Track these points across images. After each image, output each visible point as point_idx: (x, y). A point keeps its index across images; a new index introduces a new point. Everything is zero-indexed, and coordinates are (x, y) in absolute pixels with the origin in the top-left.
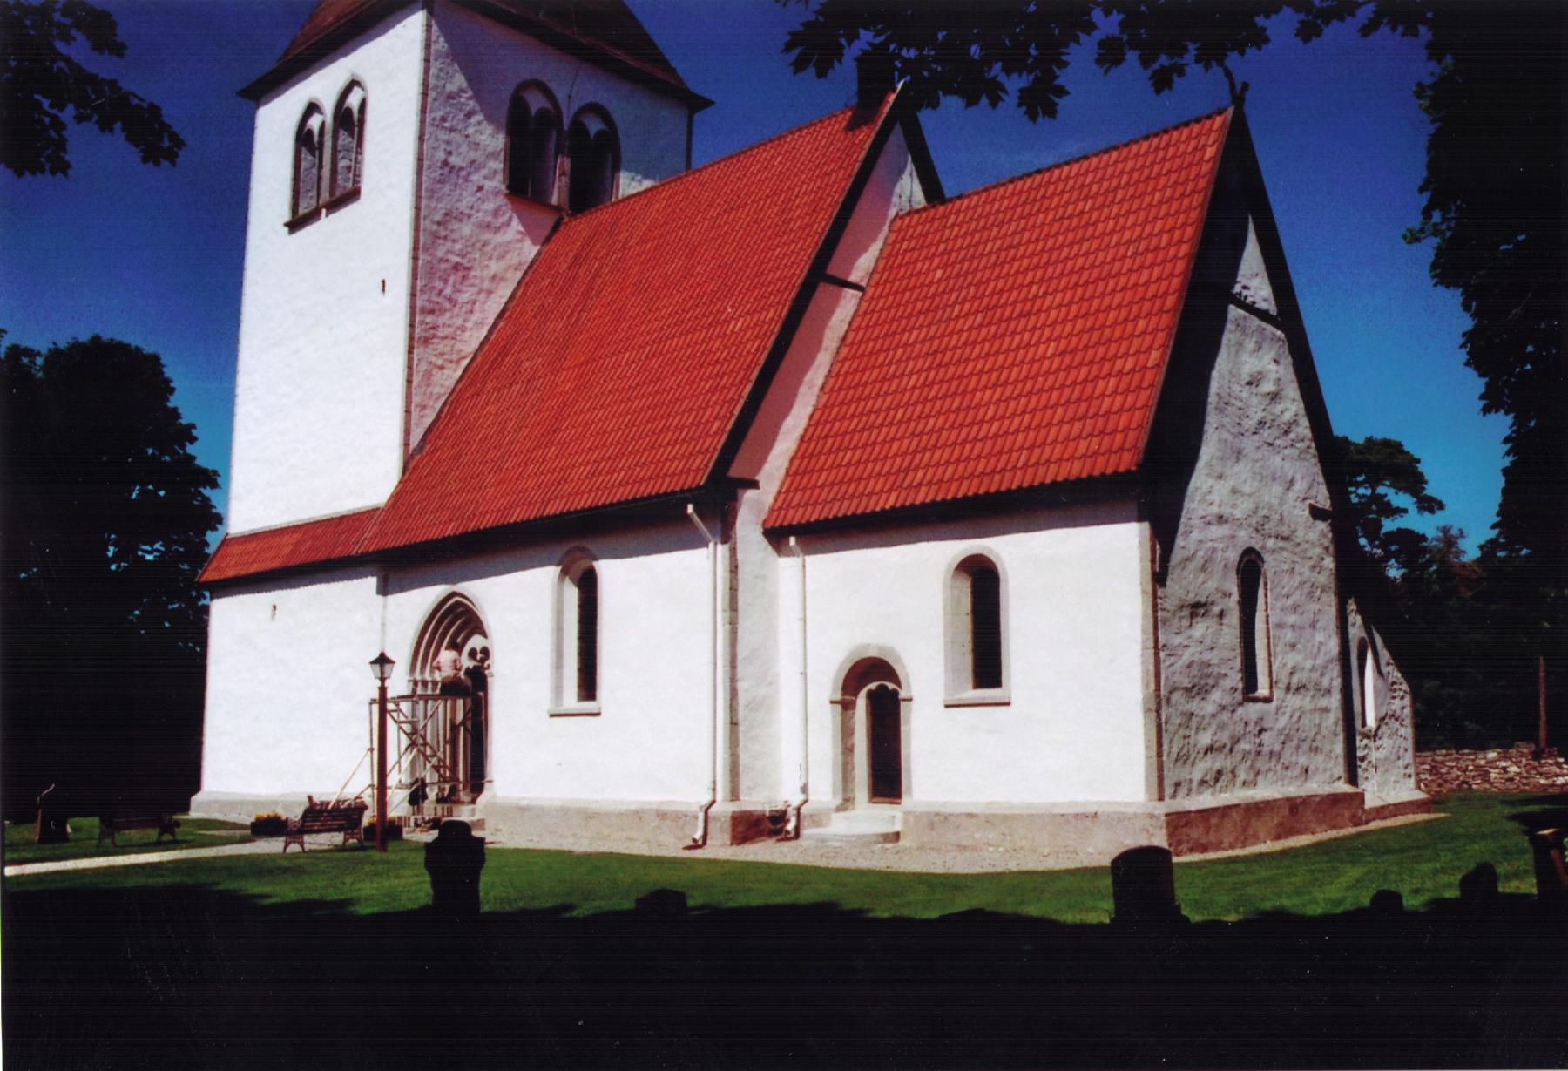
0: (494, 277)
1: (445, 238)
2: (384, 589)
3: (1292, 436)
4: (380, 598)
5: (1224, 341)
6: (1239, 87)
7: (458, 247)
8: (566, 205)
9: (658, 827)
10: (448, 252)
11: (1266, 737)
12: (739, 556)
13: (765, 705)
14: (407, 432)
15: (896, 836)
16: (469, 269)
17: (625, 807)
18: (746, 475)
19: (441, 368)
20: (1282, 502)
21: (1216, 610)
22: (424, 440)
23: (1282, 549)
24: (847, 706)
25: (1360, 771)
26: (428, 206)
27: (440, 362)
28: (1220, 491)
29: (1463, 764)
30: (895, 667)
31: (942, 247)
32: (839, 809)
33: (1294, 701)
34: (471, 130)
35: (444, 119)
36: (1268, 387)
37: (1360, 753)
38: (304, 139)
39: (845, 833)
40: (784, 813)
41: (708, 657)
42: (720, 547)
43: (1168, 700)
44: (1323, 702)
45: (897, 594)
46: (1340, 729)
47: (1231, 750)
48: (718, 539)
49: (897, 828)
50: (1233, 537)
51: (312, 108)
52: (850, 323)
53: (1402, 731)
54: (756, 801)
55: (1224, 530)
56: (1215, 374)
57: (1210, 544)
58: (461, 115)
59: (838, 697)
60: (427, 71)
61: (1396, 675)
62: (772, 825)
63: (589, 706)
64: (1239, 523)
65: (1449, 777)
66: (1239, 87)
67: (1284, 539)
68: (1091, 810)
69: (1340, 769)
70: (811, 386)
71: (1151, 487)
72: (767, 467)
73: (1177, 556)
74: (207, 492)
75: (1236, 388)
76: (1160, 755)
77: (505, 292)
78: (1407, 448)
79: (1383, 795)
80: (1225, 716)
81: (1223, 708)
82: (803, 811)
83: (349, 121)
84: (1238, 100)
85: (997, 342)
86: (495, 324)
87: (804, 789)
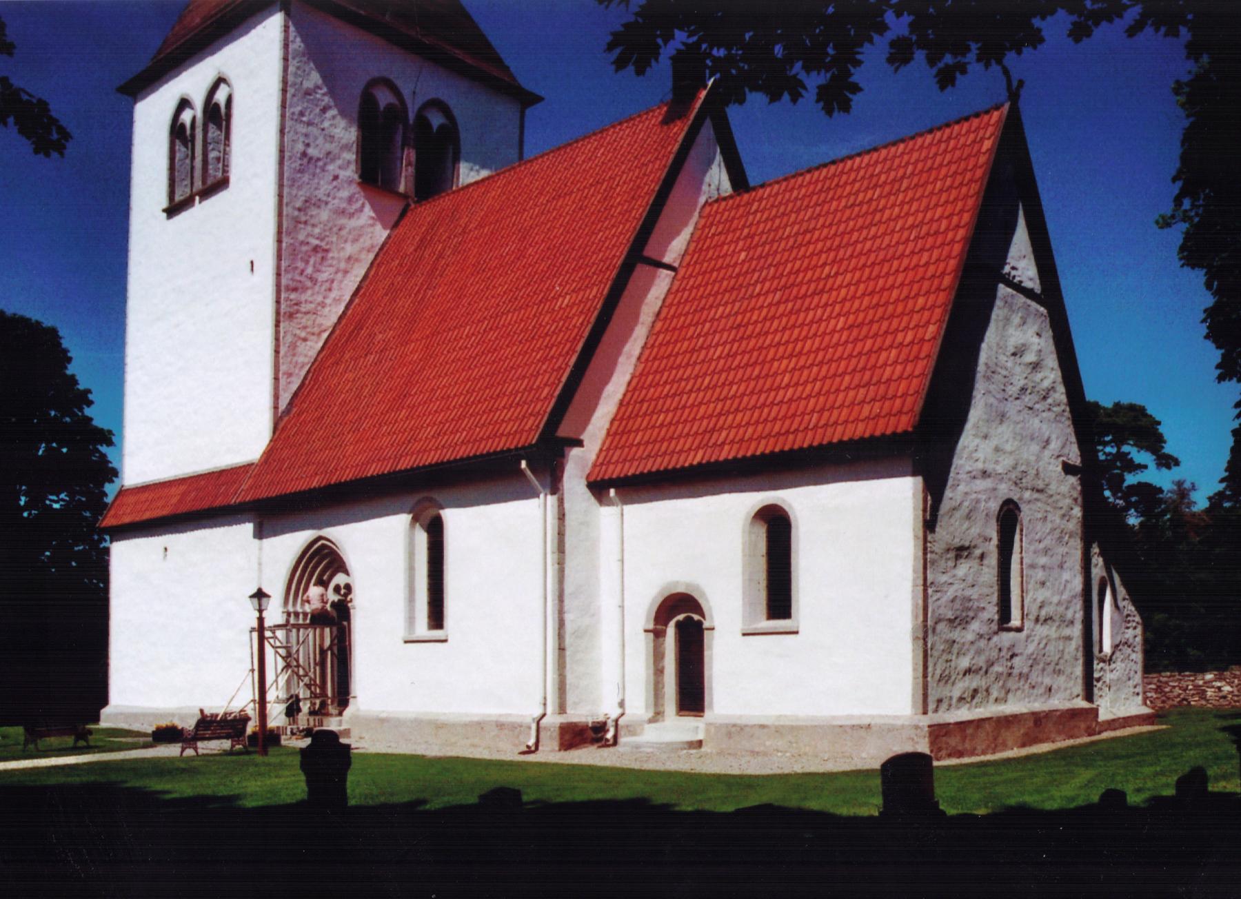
0: (349, 258)
1: (306, 223)
2: (260, 534)
3: (1050, 401)
4: (257, 541)
5: (994, 316)
6: (1015, 84)
7: (317, 231)
8: (412, 193)
10: (309, 235)
11: (1016, 660)
12: (567, 505)
13: (588, 633)
14: (276, 397)
15: (700, 744)
16: (327, 251)
18: (572, 435)
19: (305, 340)
21: (978, 552)
22: (291, 404)
23: (1037, 500)
24: (658, 634)
25: (1096, 690)
26: (289, 193)
27: (303, 334)
29: (1184, 684)
30: (701, 601)
32: (651, 721)
33: (1042, 630)
34: (326, 124)
36: (1030, 357)
37: (1096, 675)
38: (178, 132)
39: (656, 740)
40: (605, 724)
42: (549, 497)
43: (934, 630)
44: (1067, 632)
45: (701, 540)
46: (1080, 654)
47: (986, 672)
48: (548, 491)
49: (700, 737)
50: (995, 489)
51: (184, 104)
53: (1134, 656)
54: (581, 714)
56: (984, 346)
57: (974, 496)
58: (317, 110)
60: (285, 69)
63: (437, 634)
64: (1000, 478)
65: (1171, 695)
66: (1015, 84)
67: (1040, 491)
68: (866, 722)
69: (1078, 688)
71: (922, 446)
72: (590, 428)
73: (945, 506)
74: (104, 449)
75: (1003, 358)
77: (359, 272)
79: (1114, 710)
80: (982, 643)
81: (981, 636)
82: (621, 722)
83: (218, 115)
84: (1014, 96)
87: (622, 704)
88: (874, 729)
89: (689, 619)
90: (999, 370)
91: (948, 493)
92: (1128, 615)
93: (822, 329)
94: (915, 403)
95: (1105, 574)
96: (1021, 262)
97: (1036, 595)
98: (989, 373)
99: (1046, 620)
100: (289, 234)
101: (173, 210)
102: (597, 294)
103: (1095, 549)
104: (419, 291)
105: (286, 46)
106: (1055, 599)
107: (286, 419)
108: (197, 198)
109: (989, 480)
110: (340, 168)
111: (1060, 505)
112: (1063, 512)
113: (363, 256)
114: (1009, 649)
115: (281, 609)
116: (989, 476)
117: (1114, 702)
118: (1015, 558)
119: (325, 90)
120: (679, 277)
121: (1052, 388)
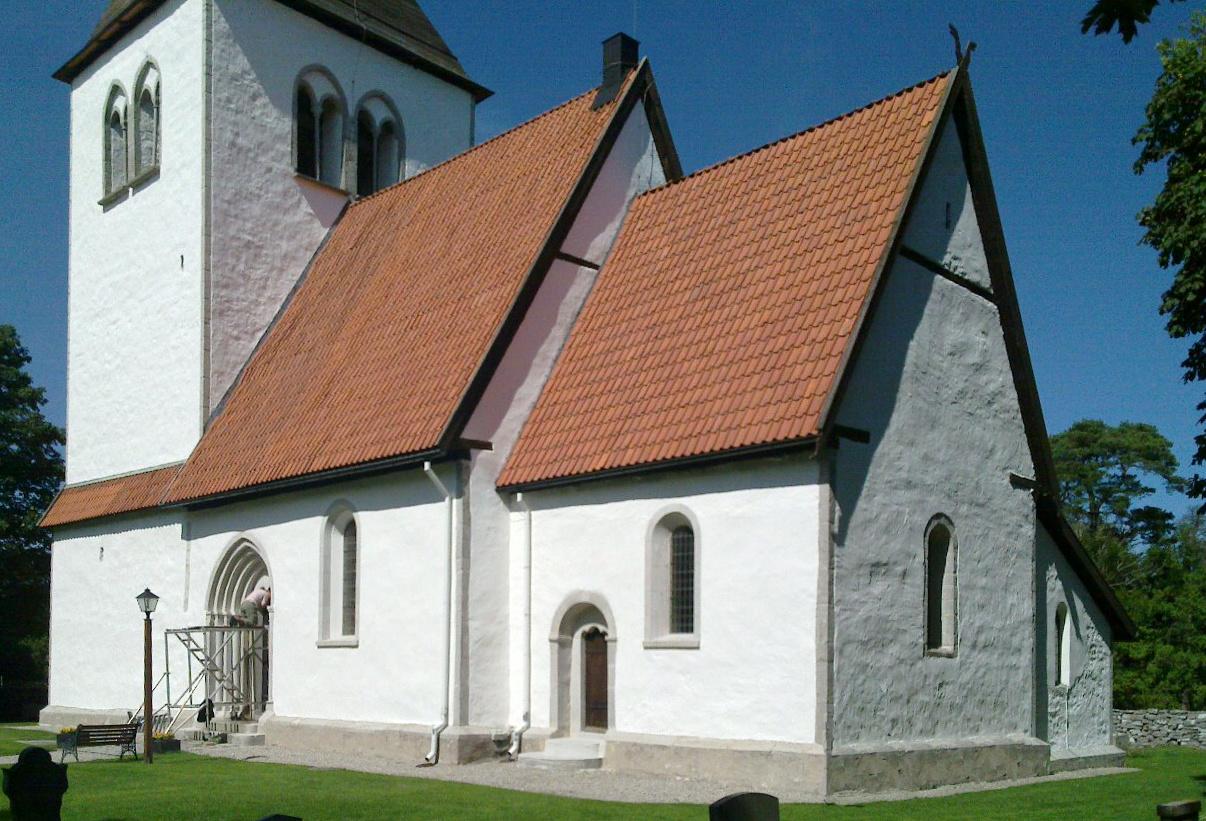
0: (285, 256)
1: (236, 216)
2: (188, 535)
3: (995, 406)
4: (184, 541)
5: (927, 311)
6: (964, 49)
7: (249, 225)
8: (354, 189)
9: (400, 747)
10: (239, 230)
11: (948, 690)
12: (472, 509)
13: (495, 642)
14: (206, 396)
15: (599, 762)
16: (261, 247)
17: (374, 728)
18: (481, 438)
19: (237, 338)
20: (979, 468)
21: (899, 569)
22: (223, 402)
23: (977, 515)
24: (563, 645)
25: (1050, 726)
26: (218, 185)
27: (235, 333)
28: (910, 459)
29: (1173, 723)
30: (604, 612)
31: (672, 224)
32: (554, 736)
33: (981, 658)
34: (257, 113)
35: (229, 101)
36: (973, 358)
37: (1050, 710)
38: (112, 120)
39: (561, 753)
40: (510, 737)
41: (443, 598)
42: (455, 501)
43: (841, 652)
44: (1013, 660)
45: (603, 548)
46: (1029, 685)
47: (908, 701)
48: (454, 494)
49: (601, 755)
50: (921, 502)
51: (116, 90)
52: (585, 300)
53: (1099, 690)
54: (484, 726)
55: (914, 495)
56: (912, 344)
57: (895, 507)
58: (246, 98)
59: (556, 636)
60: (209, 51)
61: (1097, 637)
62: (499, 747)
63: (350, 639)
64: (930, 489)
65: (1157, 733)
66: (964, 49)
67: (982, 506)
68: (767, 749)
69: (1027, 721)
70: (545, 359)
71: (834, 449)
72: (501, 431)
73: (857, 517)
74: (57, 447)
75: (937, 358)
76: (830, 701)
77: (295, 272)
78: (1160, 432)
79: (1073, 749)
80: (903, 669)
81: (902, 661)
82: (524, 736)
83: (147, 102)
84: (964, 62)
85: (708, 315)
86: (288, 300)
87: (527, 717)
88: (774, 758)
89: (596, 630)
90: (931, 370)
91: (861, 504)
92: (1092, 646)
93: (735, 327)
94: (821, 405)
95: (1064, 600)
96: (965, 249)
97: (972, 620)
98: (919, 374)
99: (985, 647)
100: (217, 227)
101: (108, 203)
102: (511, 291)
103: (1052, 572)
104: (350, 291)
105: (208, 26)
106: (998, 624)
107: (217, 419)
108: (131, 189)
109: (916, 491)
110: (273, 159)
111: (1006, 521)
112: (1009, 529)
113: (301, 254)
114: (937, 676)
115: (205, 612)
116: (915, 487)
117: (1072, 741)
118: (947, 576)
119: (253, 76)
120: (603, 274)
121: (1000, 393)
